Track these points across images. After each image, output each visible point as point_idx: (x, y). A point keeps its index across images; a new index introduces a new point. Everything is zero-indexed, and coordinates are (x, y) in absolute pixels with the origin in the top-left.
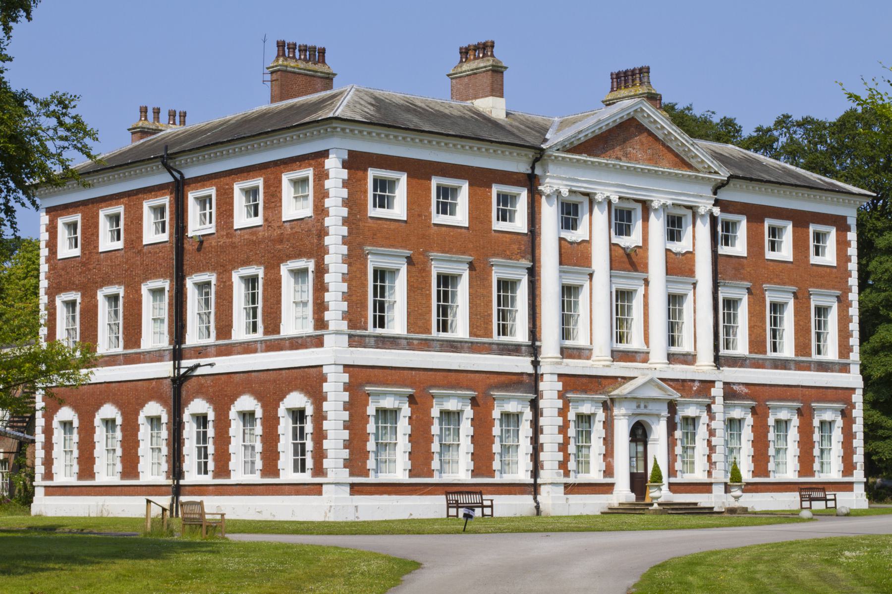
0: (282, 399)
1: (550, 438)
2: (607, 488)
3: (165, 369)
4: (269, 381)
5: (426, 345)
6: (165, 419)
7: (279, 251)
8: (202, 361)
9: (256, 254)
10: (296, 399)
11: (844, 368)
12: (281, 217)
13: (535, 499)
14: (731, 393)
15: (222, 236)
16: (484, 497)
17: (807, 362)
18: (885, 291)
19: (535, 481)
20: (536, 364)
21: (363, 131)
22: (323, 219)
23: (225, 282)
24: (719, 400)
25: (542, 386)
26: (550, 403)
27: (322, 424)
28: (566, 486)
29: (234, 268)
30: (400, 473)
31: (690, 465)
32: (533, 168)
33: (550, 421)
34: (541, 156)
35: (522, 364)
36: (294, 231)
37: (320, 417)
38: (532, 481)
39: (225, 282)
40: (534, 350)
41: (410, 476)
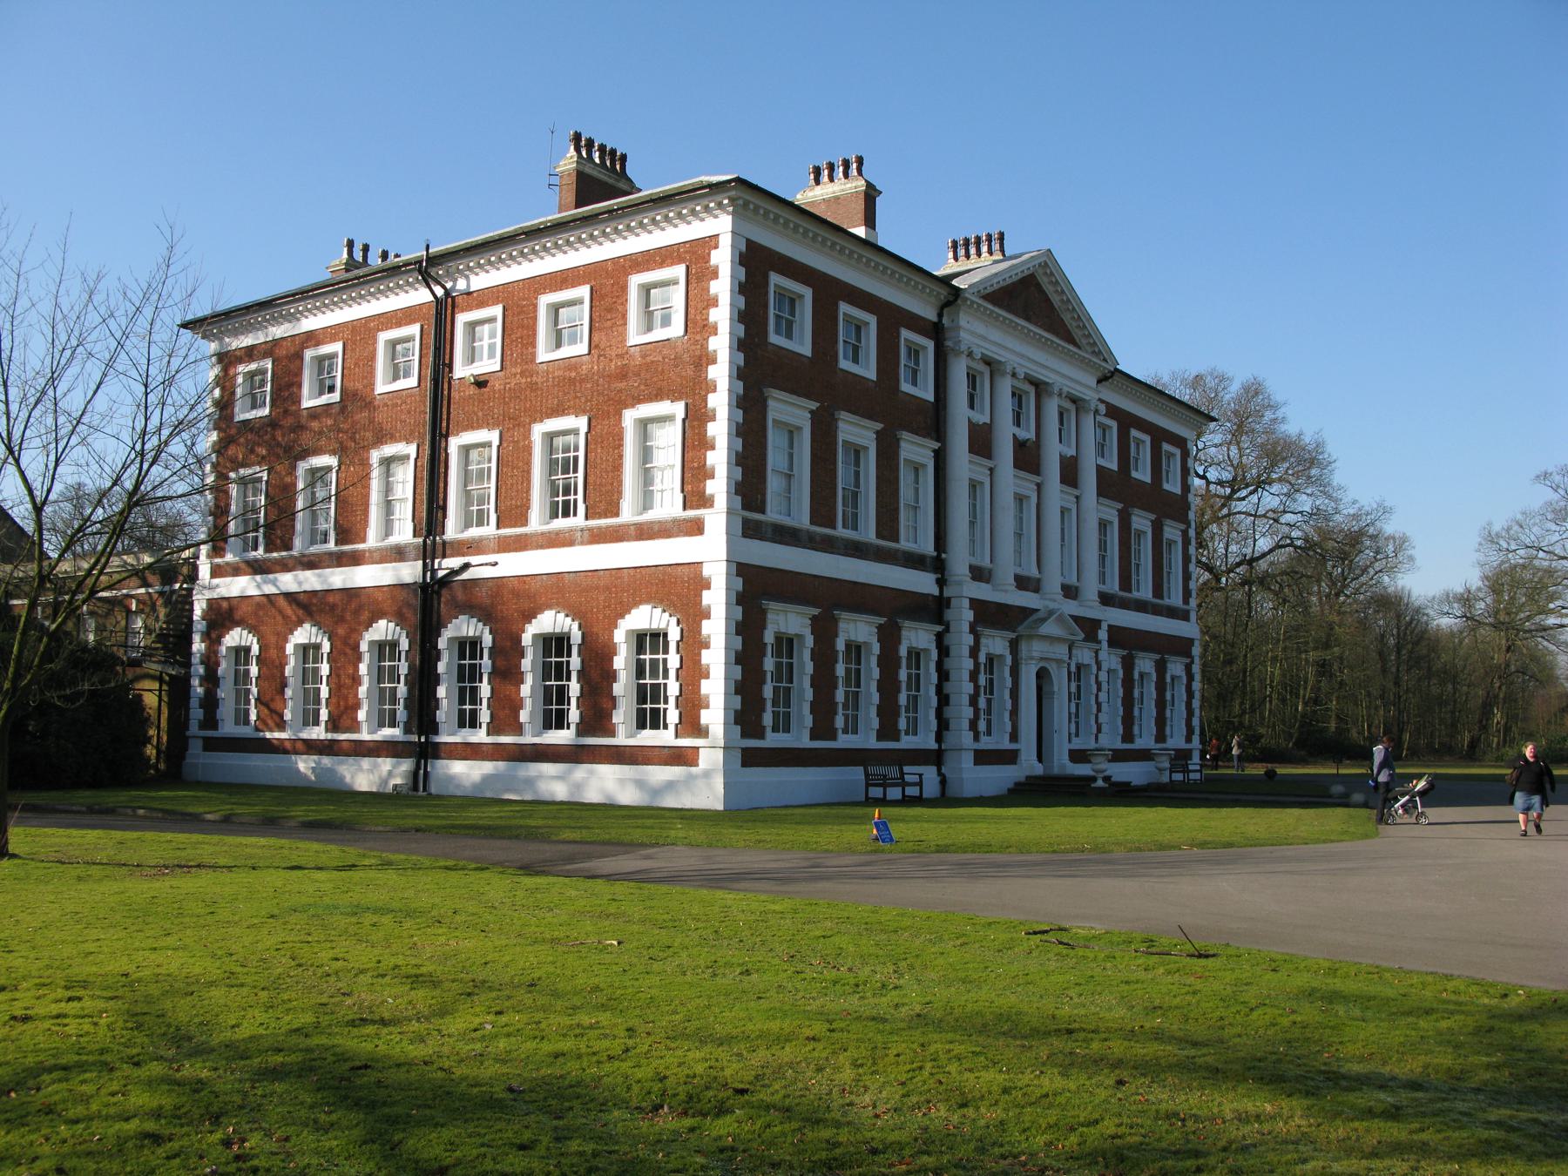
0: (622, 616)
1: (962, 687)
2: (1009, 757)
3: (410, 572)
4: (597, 588)
5: (828, 545)
6: (404, 644)
7: (620, 391)
8: (474, 560)
9: (576, 397)
10: (643, 617)
11: (1185, 616)
12: (624, 340)
13: (940, 773)
14: (1120, 637)
15: (515, 375)
16: (906, 769)
17: (747, 627)
18: (40, 666)
19: (940, 746)
20: (941, 583)
21: (769, 211)
22: (707, 340)
23: (518, 442)
24: (1105, 645)
25: (949, 615)
26: (962, 639)
27: (700, 655)
28: (976, 752)
29: (535, 421)
30: (799, 737)
31: (852, 727)
32: (940, 315)
33: (962, 664)
34: (956, 300)
35: (923, 583)
36: (649, 359)
37: (693, 643)
38: (935, 746)
39: (518, 442)
40: (937, 565)
41: (812, 738)
